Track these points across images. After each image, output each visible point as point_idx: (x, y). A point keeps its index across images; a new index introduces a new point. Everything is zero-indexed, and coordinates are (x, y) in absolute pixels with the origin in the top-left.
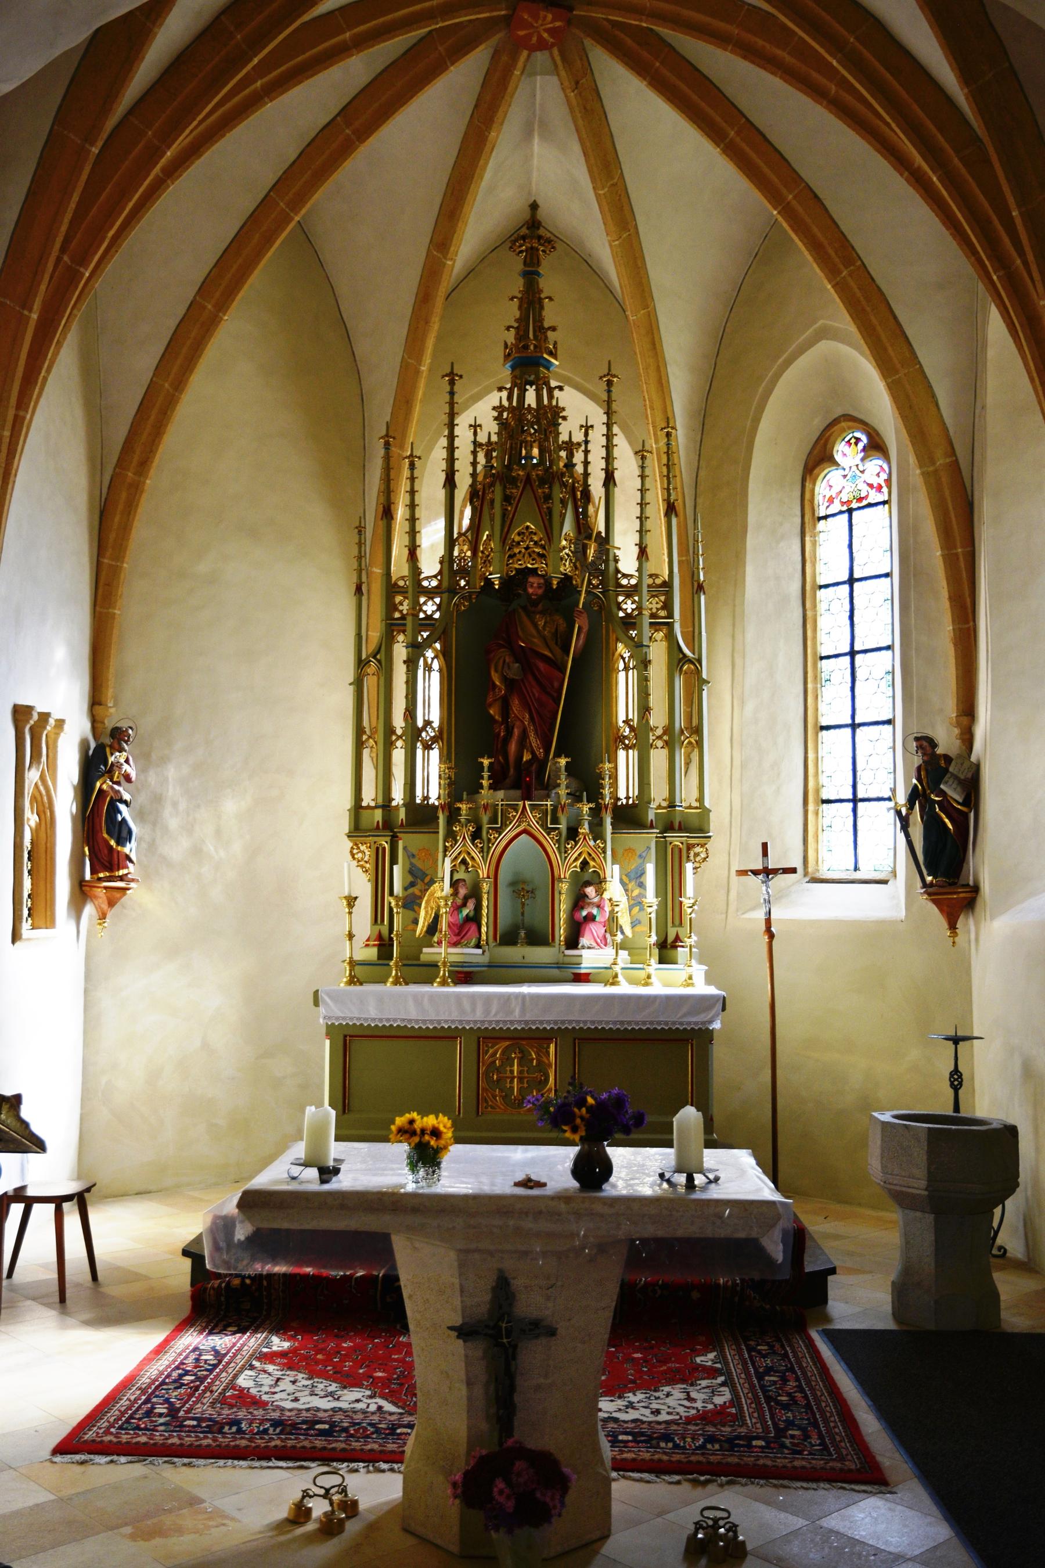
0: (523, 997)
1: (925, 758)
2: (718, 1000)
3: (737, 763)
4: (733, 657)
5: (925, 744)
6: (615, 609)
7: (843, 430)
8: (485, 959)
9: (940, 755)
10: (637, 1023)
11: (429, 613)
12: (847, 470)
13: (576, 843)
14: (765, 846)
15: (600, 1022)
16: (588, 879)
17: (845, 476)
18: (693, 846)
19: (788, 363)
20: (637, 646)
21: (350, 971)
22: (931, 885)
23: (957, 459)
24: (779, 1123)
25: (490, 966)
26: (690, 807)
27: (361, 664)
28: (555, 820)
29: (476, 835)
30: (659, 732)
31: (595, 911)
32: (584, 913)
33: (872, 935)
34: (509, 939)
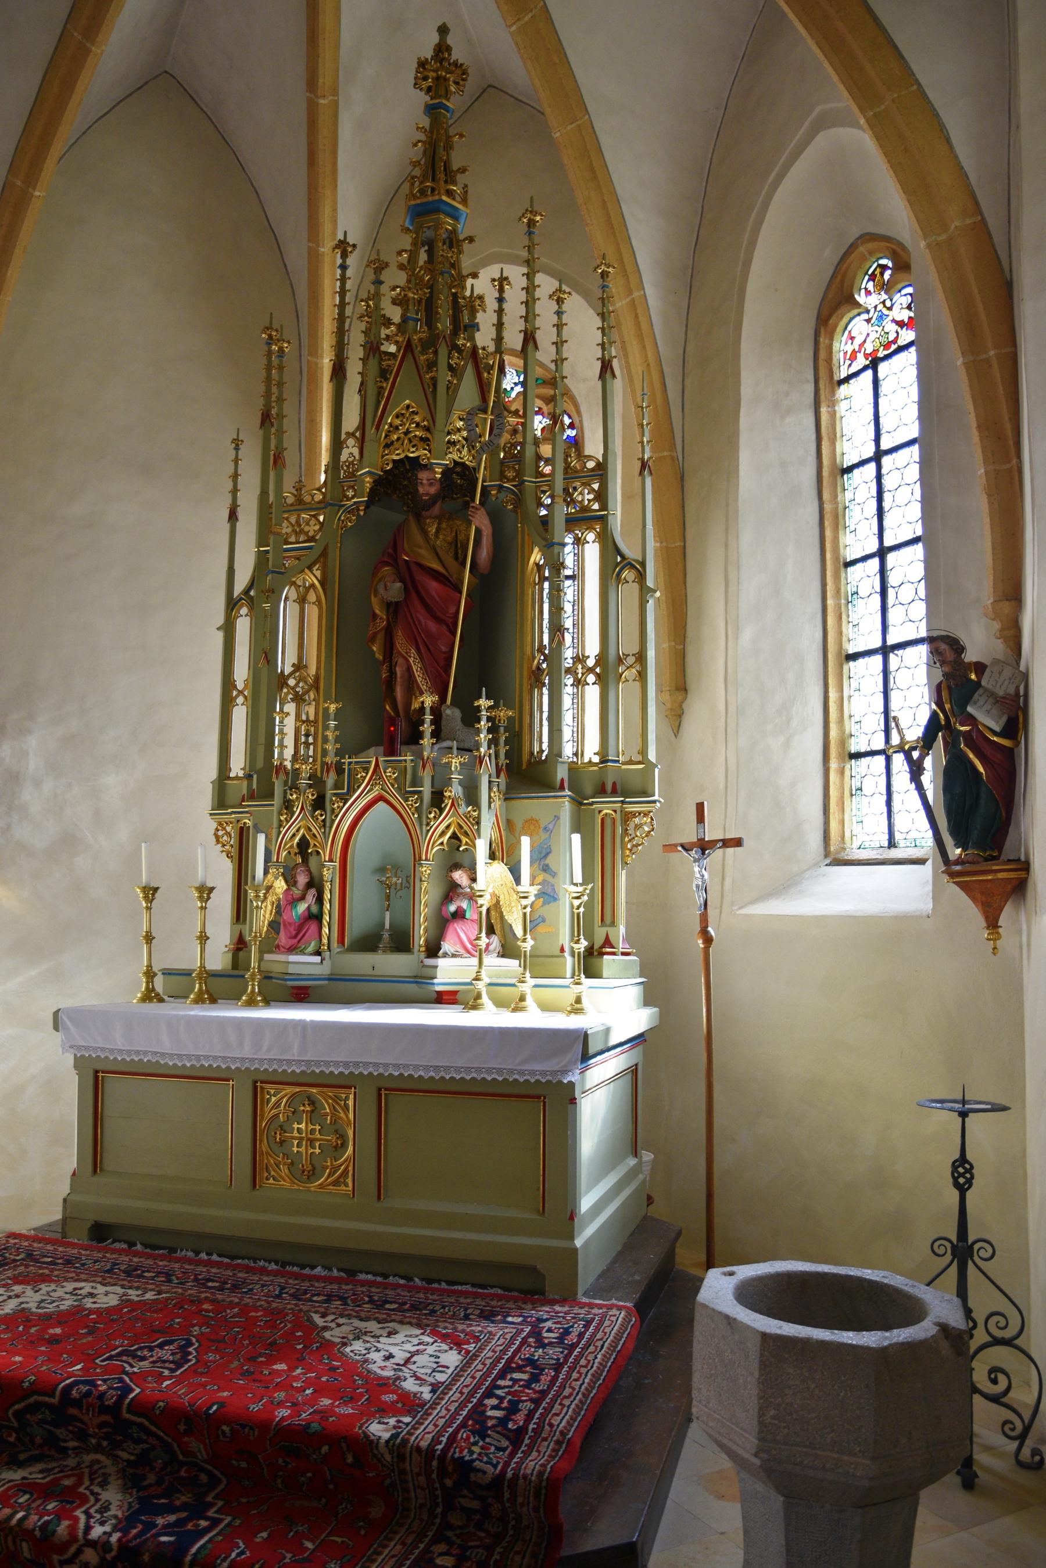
0: (302, 1025)
1: (946, 669)
2: (577, 1038)
3: (732, 708)
4: (726, 571)
5: (943, 646)
6: (531, 504)
7: (863, 259)
8: (325, 969)
9: (969, 664)
10: (458, 1069)
11: (311, 534)
12: (872, 311)
13: (441, 811)
14: (700, 807)
15: (406, 1066)
16: (457, 856)
17: (868, 321)
18: (634, 815)
19: (781, 176)
20: (551, 547)
21: (147, 983)
22: (959, 861)
23: (983, 219)
24: (717, 1221)
25: (331, 979)
26: (631, 762)
27: (232, 604)
28: (416, 781)
29: (319, 803)
30: (591, 663)
31: (464, 905)
32: (452, 908)
33: (882, 936)
34: (368, 943)
